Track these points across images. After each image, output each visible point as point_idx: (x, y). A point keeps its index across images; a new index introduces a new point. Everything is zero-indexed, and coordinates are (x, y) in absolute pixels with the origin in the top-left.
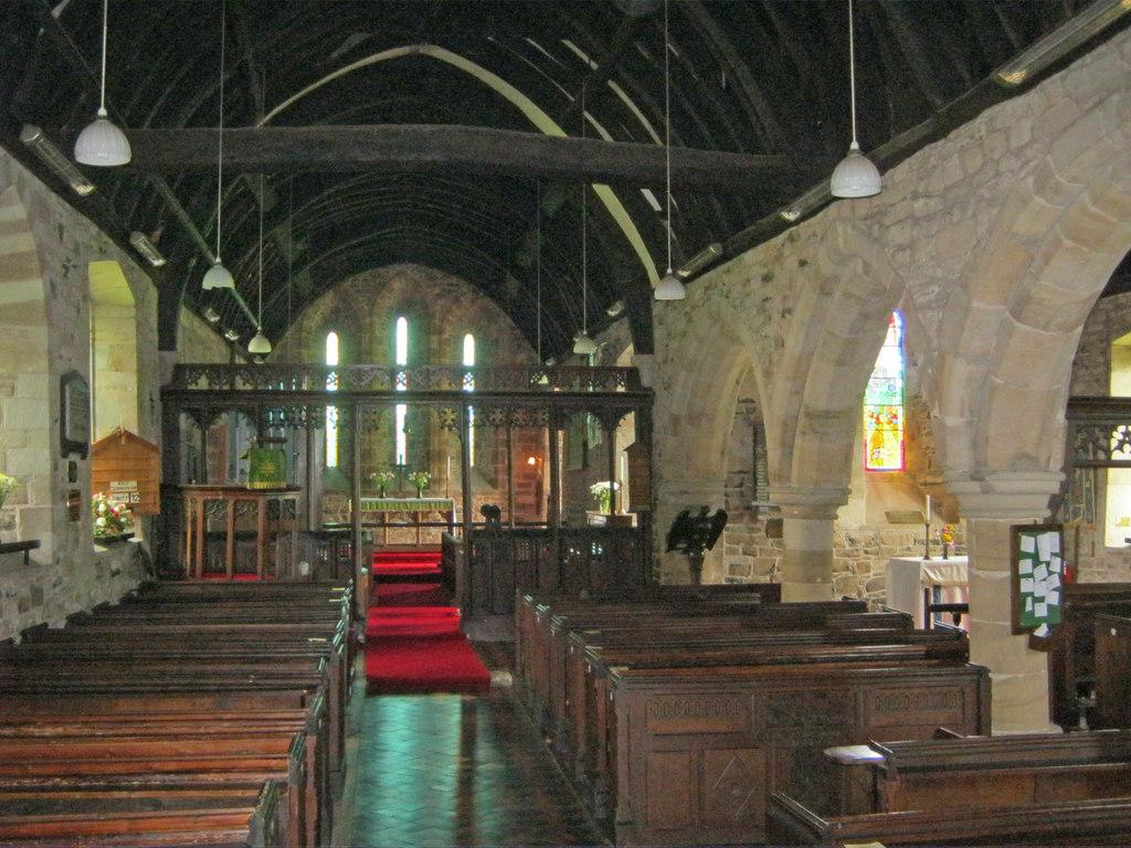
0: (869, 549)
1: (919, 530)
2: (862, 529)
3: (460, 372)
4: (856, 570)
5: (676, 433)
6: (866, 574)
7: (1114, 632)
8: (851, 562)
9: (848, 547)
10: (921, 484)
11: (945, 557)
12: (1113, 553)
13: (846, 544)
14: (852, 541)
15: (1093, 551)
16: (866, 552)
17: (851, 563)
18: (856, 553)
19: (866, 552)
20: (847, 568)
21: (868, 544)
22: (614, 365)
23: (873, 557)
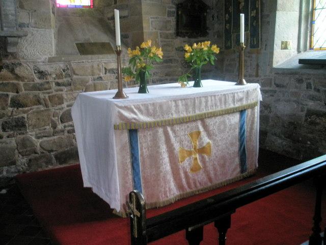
0: (60, 81)
1: (109, 61)
2: (51, 60)
3: (210, 53)
4: (50, 104)
5: (295, 101)
6: (60, 106)
7: (300, 139)
8: (42, 95)
9: (37, 81)
10: (109, 19)
11: (143, 90)
12: (283, 74)
13: (35, 77)
14: (42, 74)
15: (257, 72)
16: (58, 84)
17: (42, 96)
18: (46, 86)
19: (58, 84)
20: (38, 102)
21: (59, 76)
22: (7, 189)
23: (65, 89)
